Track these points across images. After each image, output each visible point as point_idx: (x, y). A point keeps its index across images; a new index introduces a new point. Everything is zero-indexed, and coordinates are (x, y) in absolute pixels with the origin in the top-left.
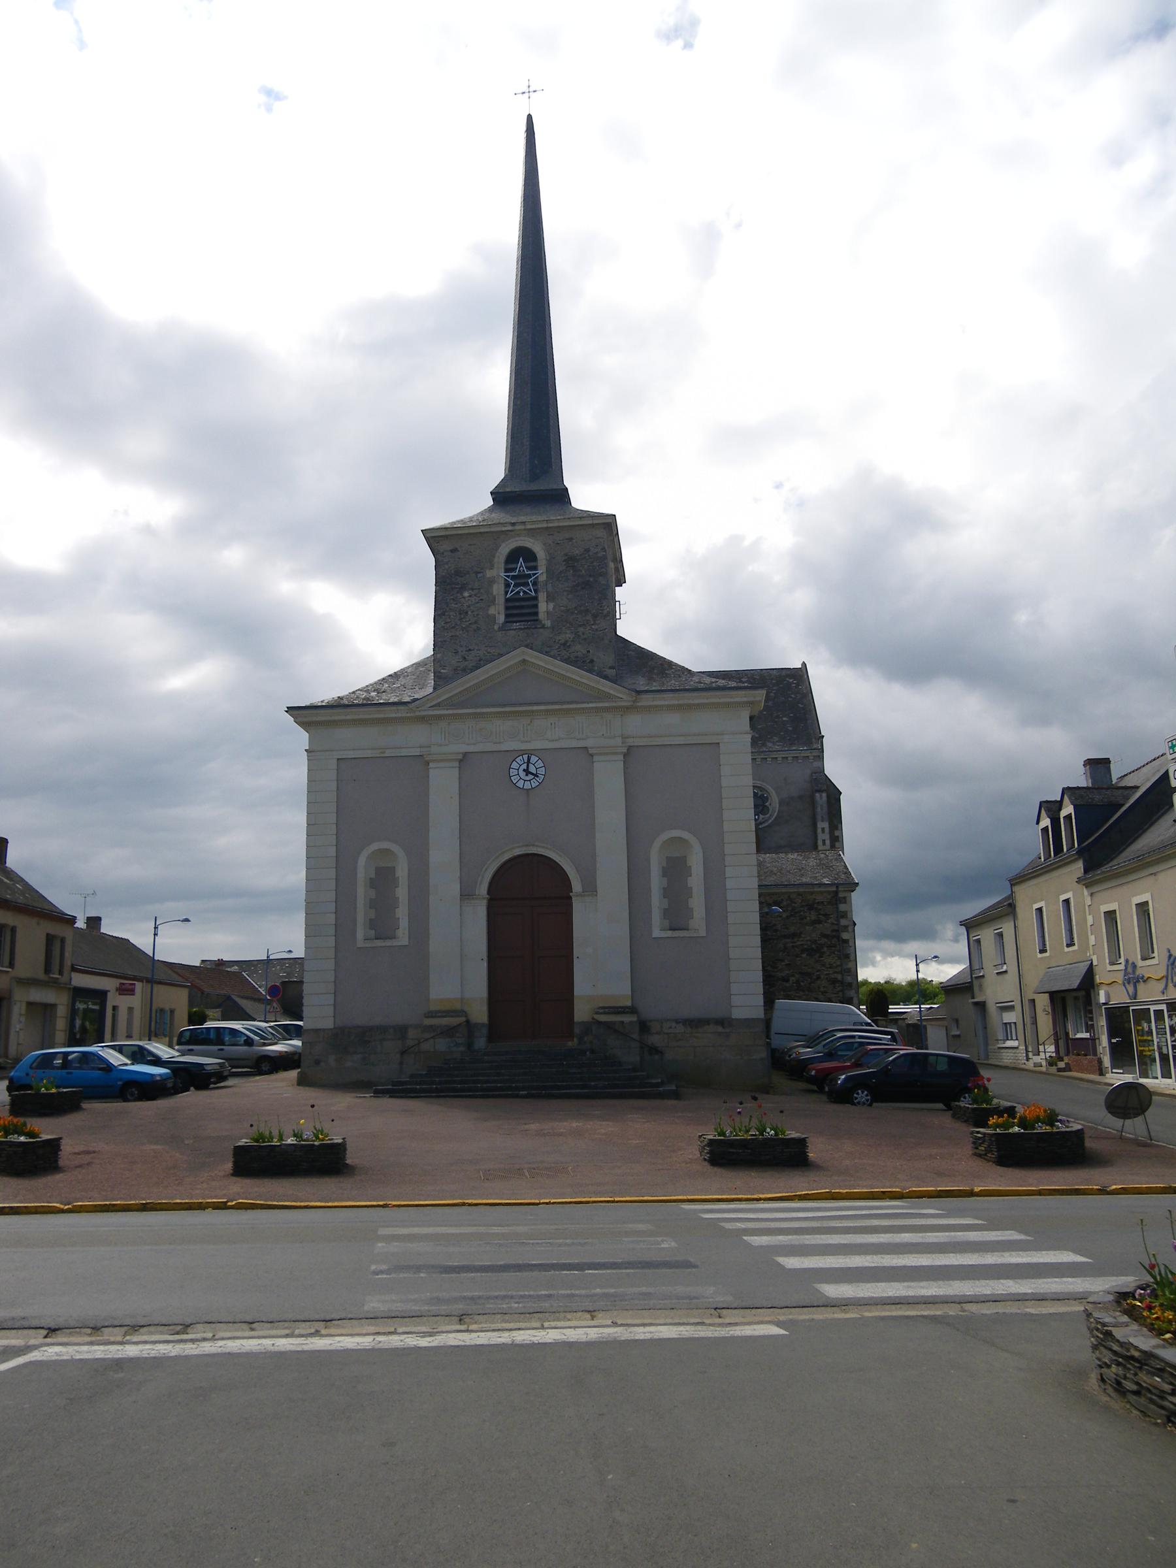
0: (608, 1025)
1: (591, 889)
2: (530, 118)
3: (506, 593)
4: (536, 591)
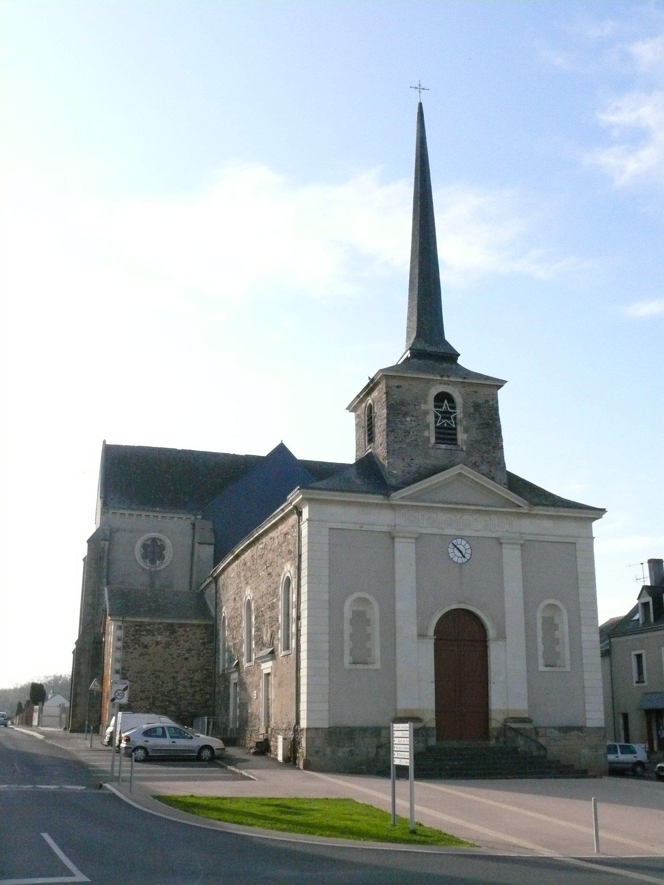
0: (516, 730)
1: (502, 636)
2: (420, 104)
3: (436, 422)
4: (456, 424)
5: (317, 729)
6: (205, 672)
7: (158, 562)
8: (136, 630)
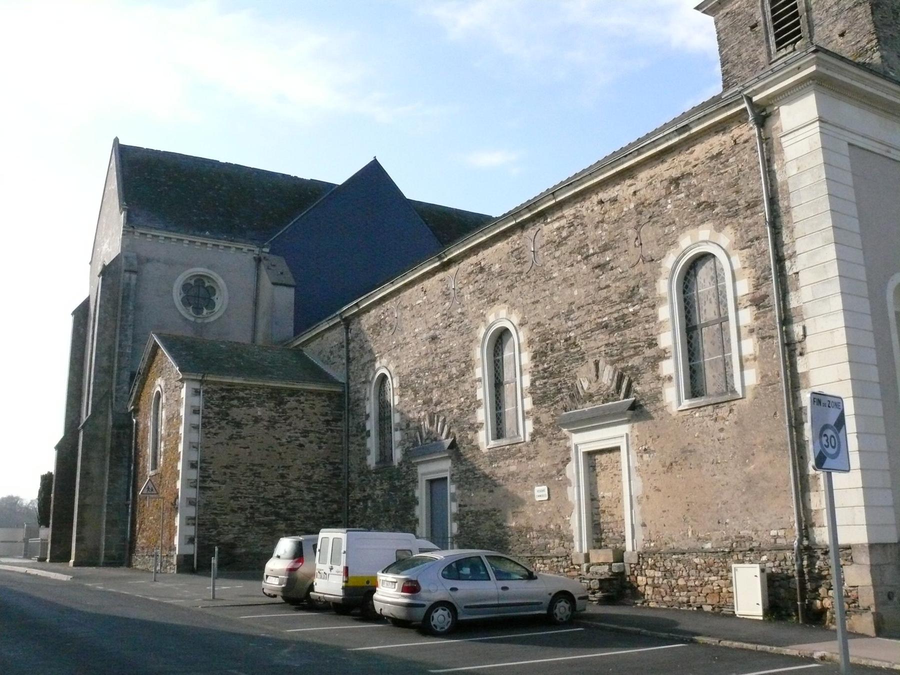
5: (884, 545)
6: (329, 467)
7: (205, 311)
8: (223, 398)
